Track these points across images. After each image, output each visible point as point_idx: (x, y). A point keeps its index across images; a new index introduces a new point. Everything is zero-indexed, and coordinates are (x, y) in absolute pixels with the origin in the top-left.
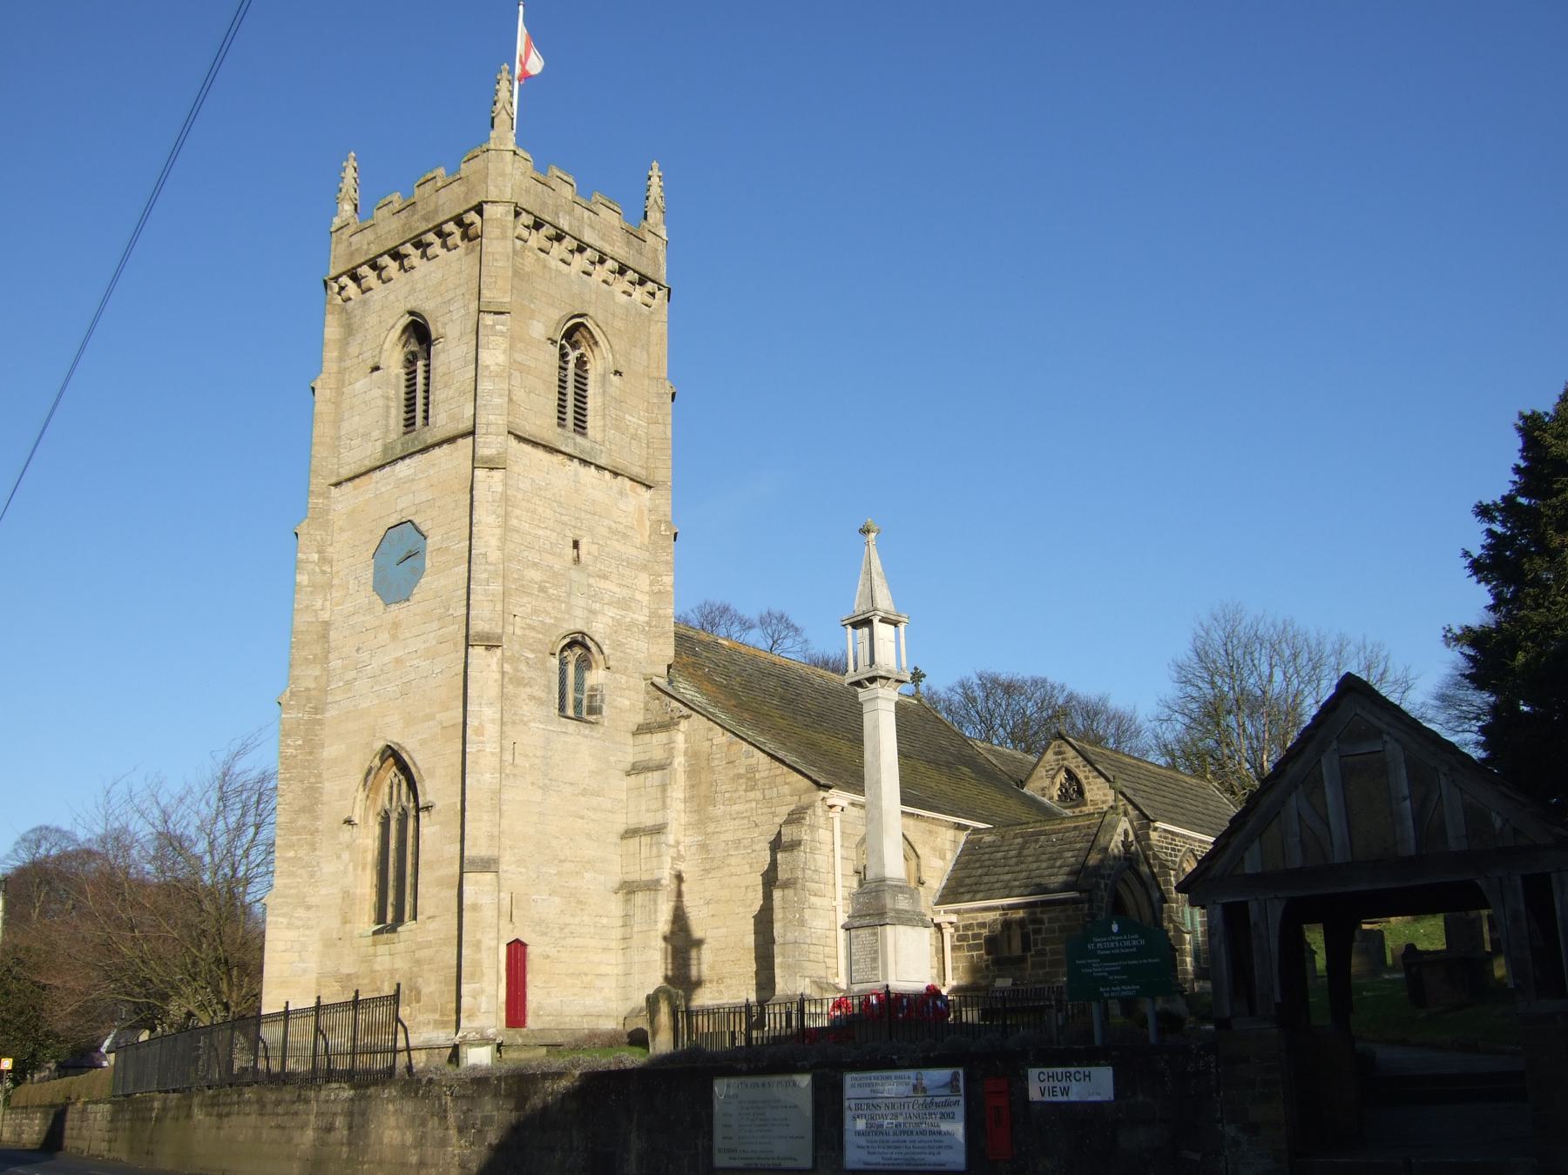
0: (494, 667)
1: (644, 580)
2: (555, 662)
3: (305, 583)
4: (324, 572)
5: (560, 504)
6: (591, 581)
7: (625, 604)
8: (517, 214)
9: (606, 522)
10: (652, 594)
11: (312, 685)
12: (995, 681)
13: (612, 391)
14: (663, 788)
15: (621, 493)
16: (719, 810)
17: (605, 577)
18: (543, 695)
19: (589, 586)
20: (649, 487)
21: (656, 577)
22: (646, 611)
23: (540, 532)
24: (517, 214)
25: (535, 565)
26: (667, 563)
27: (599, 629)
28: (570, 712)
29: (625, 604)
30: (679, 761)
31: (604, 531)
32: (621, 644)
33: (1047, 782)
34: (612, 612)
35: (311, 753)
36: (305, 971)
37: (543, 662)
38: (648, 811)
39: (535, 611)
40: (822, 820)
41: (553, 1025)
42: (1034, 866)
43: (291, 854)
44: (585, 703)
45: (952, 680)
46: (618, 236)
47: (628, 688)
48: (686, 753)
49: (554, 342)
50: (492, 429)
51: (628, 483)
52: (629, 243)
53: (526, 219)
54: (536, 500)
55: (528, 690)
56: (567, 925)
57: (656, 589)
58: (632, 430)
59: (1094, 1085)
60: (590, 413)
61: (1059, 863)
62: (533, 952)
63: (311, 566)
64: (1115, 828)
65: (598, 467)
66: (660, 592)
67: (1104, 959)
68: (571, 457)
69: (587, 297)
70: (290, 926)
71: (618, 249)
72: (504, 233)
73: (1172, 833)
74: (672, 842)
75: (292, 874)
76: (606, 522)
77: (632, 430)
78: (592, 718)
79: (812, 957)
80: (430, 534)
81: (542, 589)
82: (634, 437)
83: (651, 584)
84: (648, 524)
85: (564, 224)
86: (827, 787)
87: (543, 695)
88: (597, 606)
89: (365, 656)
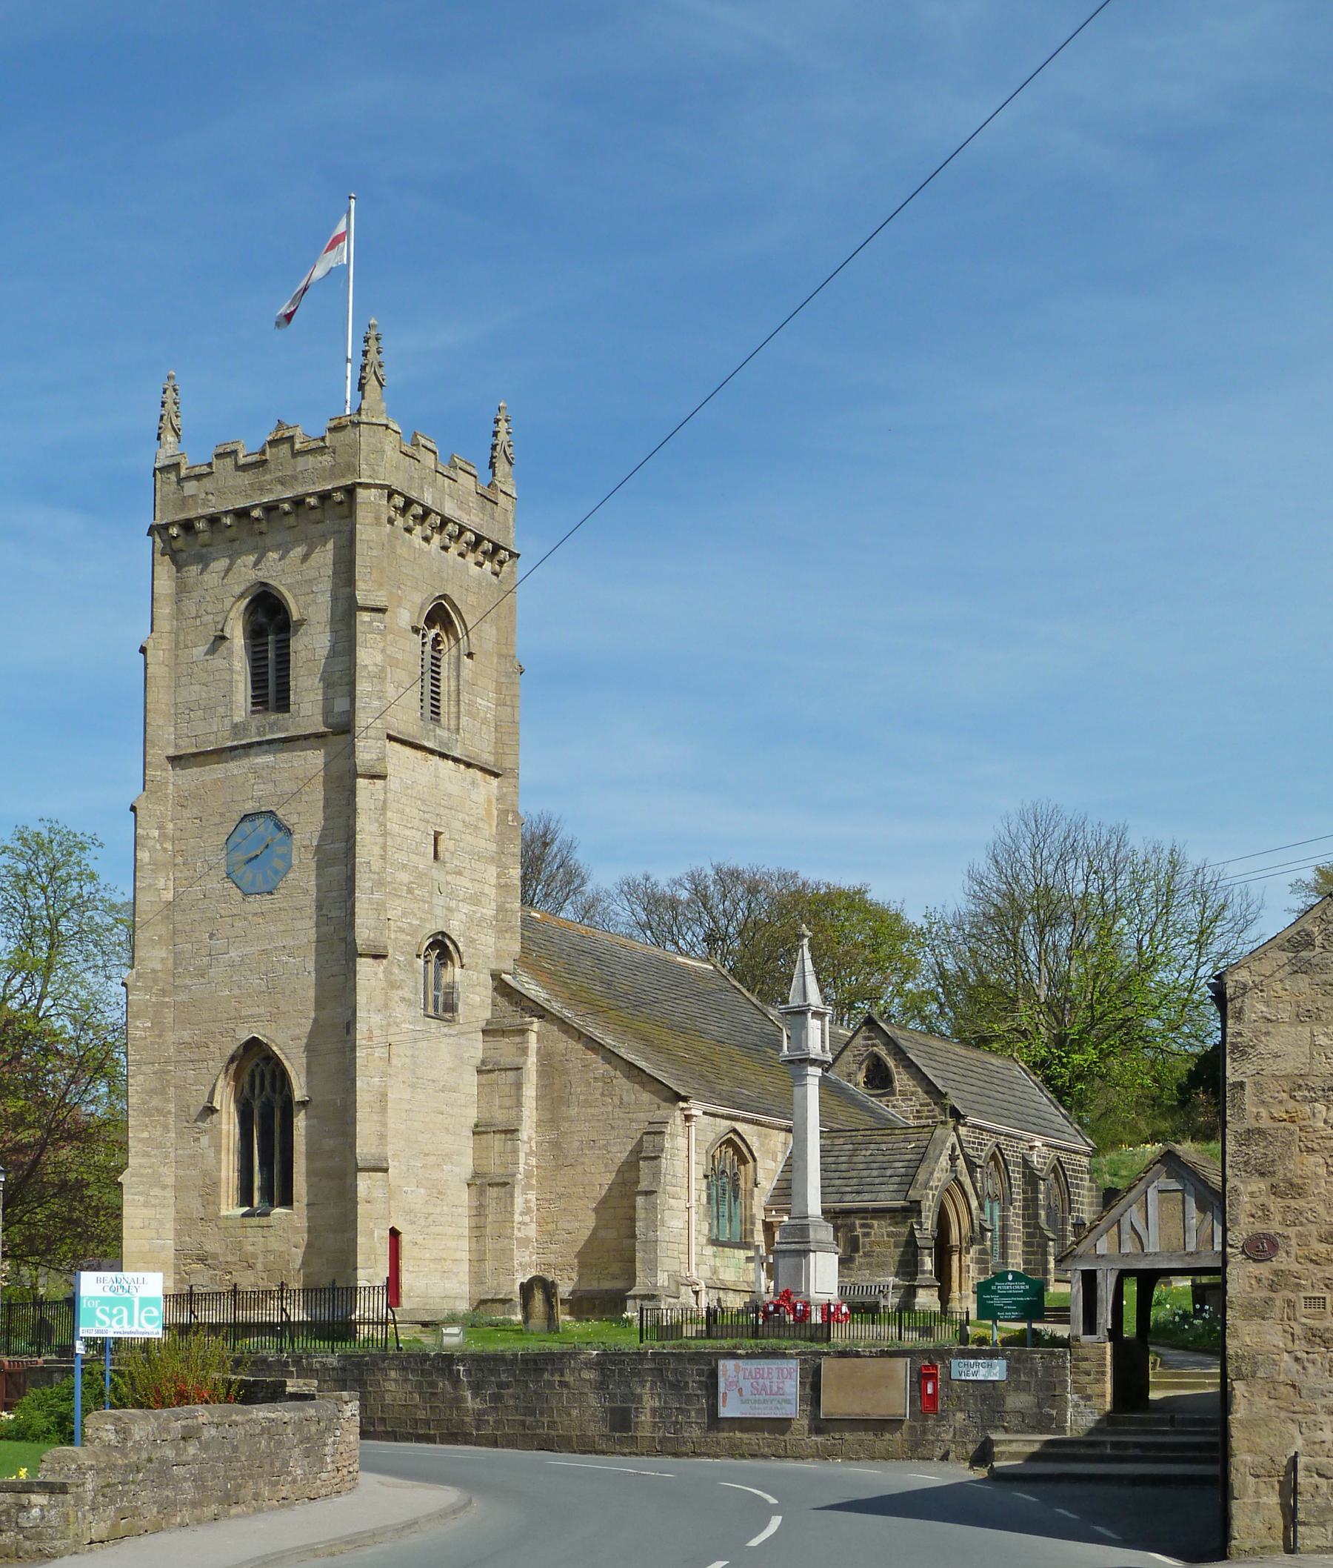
0: (381, 976)
1: (492, 871)
2: (421, 962)
3: (147, 860)
4: (165, 850)
5: (424, 801)
6: (449, 878)
7: (475, 899)
8: (390, 496)
9: (461, 816)
10: (499, 886)
11: (159, 967)
12: (735, 875)
13: (465, 673)
14: (518, 1086)
15: (473, 783)
16: (573, 1111)
17: (460, 873)
18: (412, 996)
19: (448, 883)
20: (496, 775)
21: (502, 867)
22: (493, 905)
23: (408, 832)
24: (390, 496)
25: (404, 866)
26: (514, 855)
27: (456, 929)
28: (431, 1011)
29: (475, 899)
30: (532, 1061)
31: (458, 825)
32: (473, 941)
33: (855, 1067)
34: (465, 908)
35: (160, 1036)
36: (163, 1247)
37: (411, 964)
38: (500, 1107)
39: (404, 914)
40: (680, 1129)
41: (421, 1306)
42: (865, 1173)
43: (145, 1135)
44: (441, 1000)
45: (680, 871)
46: (473, 500)
47: (478, 984)
48: (538, 1052)
49: (416, 630)
50: (371, 733)
51: (479, 774)
52: (483, 509)
53: (399, 501)
54: (404, 800)
55: (400, 992)
56: (430, 1214)
57: (503, 881)
58: (482, 715)
59: (995, 1371)
60: (444, 698)
61: (889, 1172)
62: (405, 1239)
63: (151, 843)
64: (944, 1142)
65: (456, 760)
66: (506, 885)
67: (1002, 1296)
68: (432, 752)
69: (445, 575)
70: (146, 1205)
71: (473, 518)
72: (377, 518)
73: (981, 1128)
74: (525, 1138)
75: (146, 1155)
76: (461, 816)
77: (482, 715)
78: (448, 1016)
79: (670, 1253)
80: (297, 829)
81: (410, 891)
82: (484, 721)
83: (499, 876)
84: (495, 813)
85: (428, 499)
86: (685, 1099)
87: (412, 996)
88: (453, 904)
89: (219, 944)
